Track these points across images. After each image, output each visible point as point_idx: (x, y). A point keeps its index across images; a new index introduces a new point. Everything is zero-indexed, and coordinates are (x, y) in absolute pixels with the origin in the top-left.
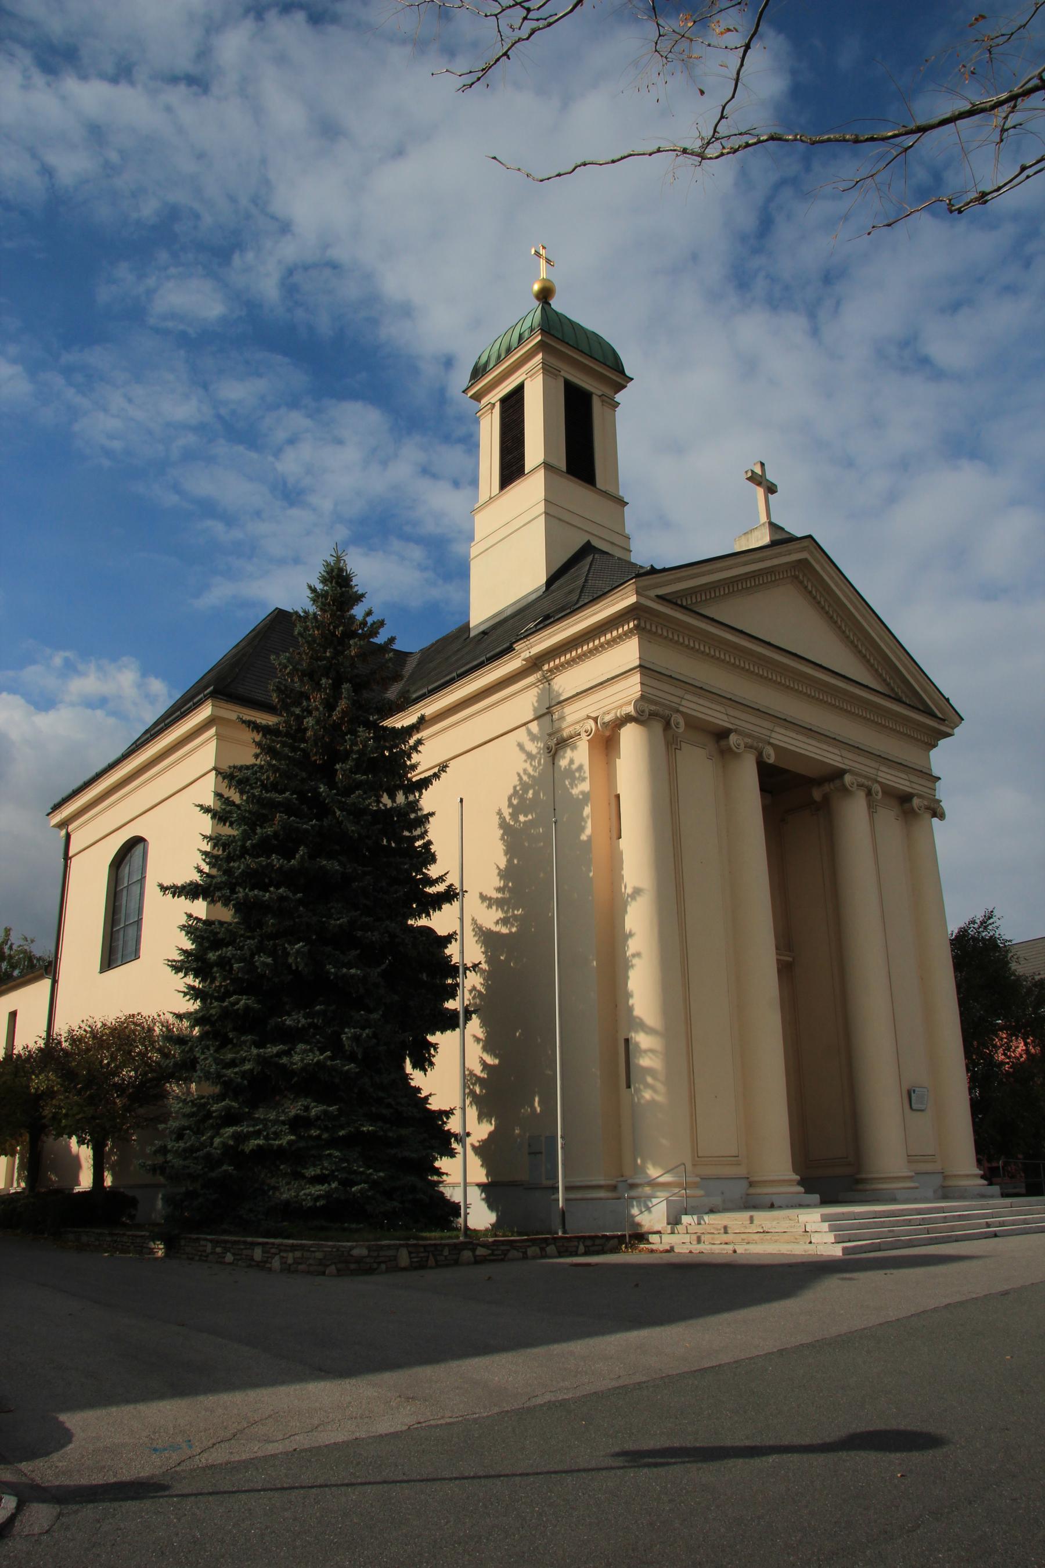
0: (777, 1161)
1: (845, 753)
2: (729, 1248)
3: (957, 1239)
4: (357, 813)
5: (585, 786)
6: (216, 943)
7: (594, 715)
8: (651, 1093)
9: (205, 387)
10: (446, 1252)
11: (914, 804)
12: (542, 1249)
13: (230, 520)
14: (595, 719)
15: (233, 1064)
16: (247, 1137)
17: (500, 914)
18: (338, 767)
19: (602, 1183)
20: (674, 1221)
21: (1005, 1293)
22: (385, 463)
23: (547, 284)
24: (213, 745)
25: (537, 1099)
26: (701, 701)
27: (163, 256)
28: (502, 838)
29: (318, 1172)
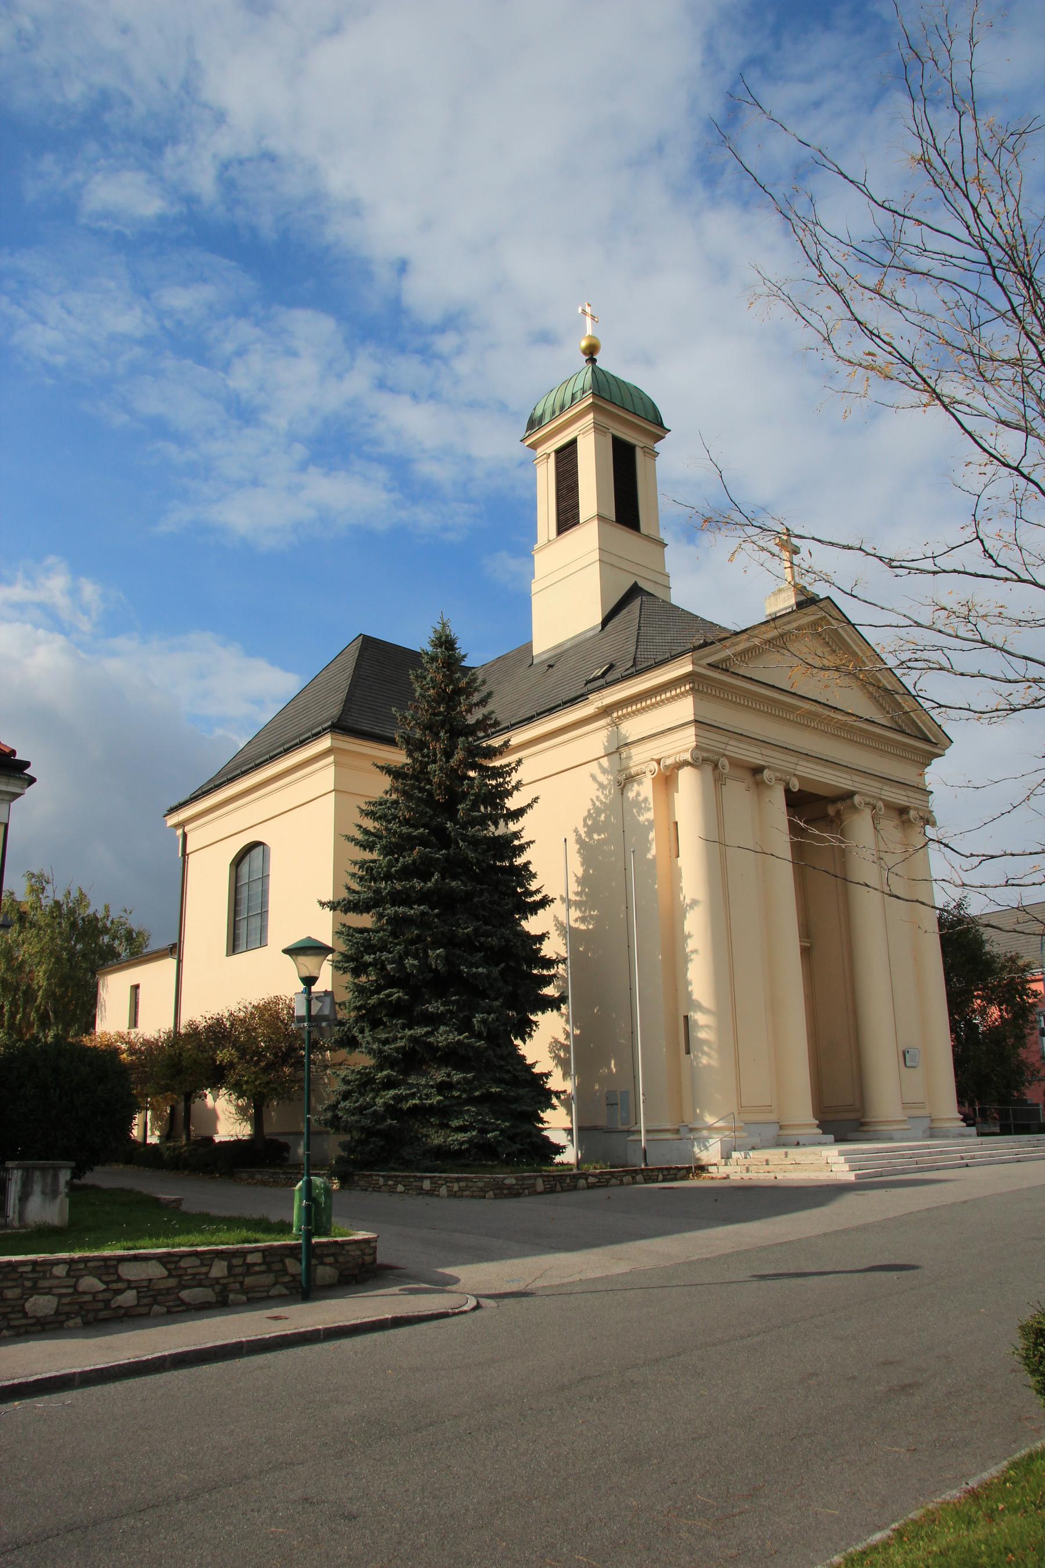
0: (801, 1109)
1: (855, 778)
2: (772, 1175)
3: (945, 1167)
4: (475, 842)
5: (650, 815)
6: (370, 948)
7: (657, 757)
8: (706, 1059)
9: (146, 294)
10: (568, 1181)
11: (910, 815)
12: (633, 1178)
13: (181, 439)
14: (658, 762)
15: (386, 1042)
16: (406, 1098)
17: (578, 914)
18: (459, 807)
19: (669, 1127)
20: (727, 1157)
21: (965, 1202)
22: (340, 376)
23: (594, 342)
24: (331, 771)
25: (613, 1062)
26: (751, 748)
27: (92, 148)
28: (579, 852)
29: (461, 1123)
